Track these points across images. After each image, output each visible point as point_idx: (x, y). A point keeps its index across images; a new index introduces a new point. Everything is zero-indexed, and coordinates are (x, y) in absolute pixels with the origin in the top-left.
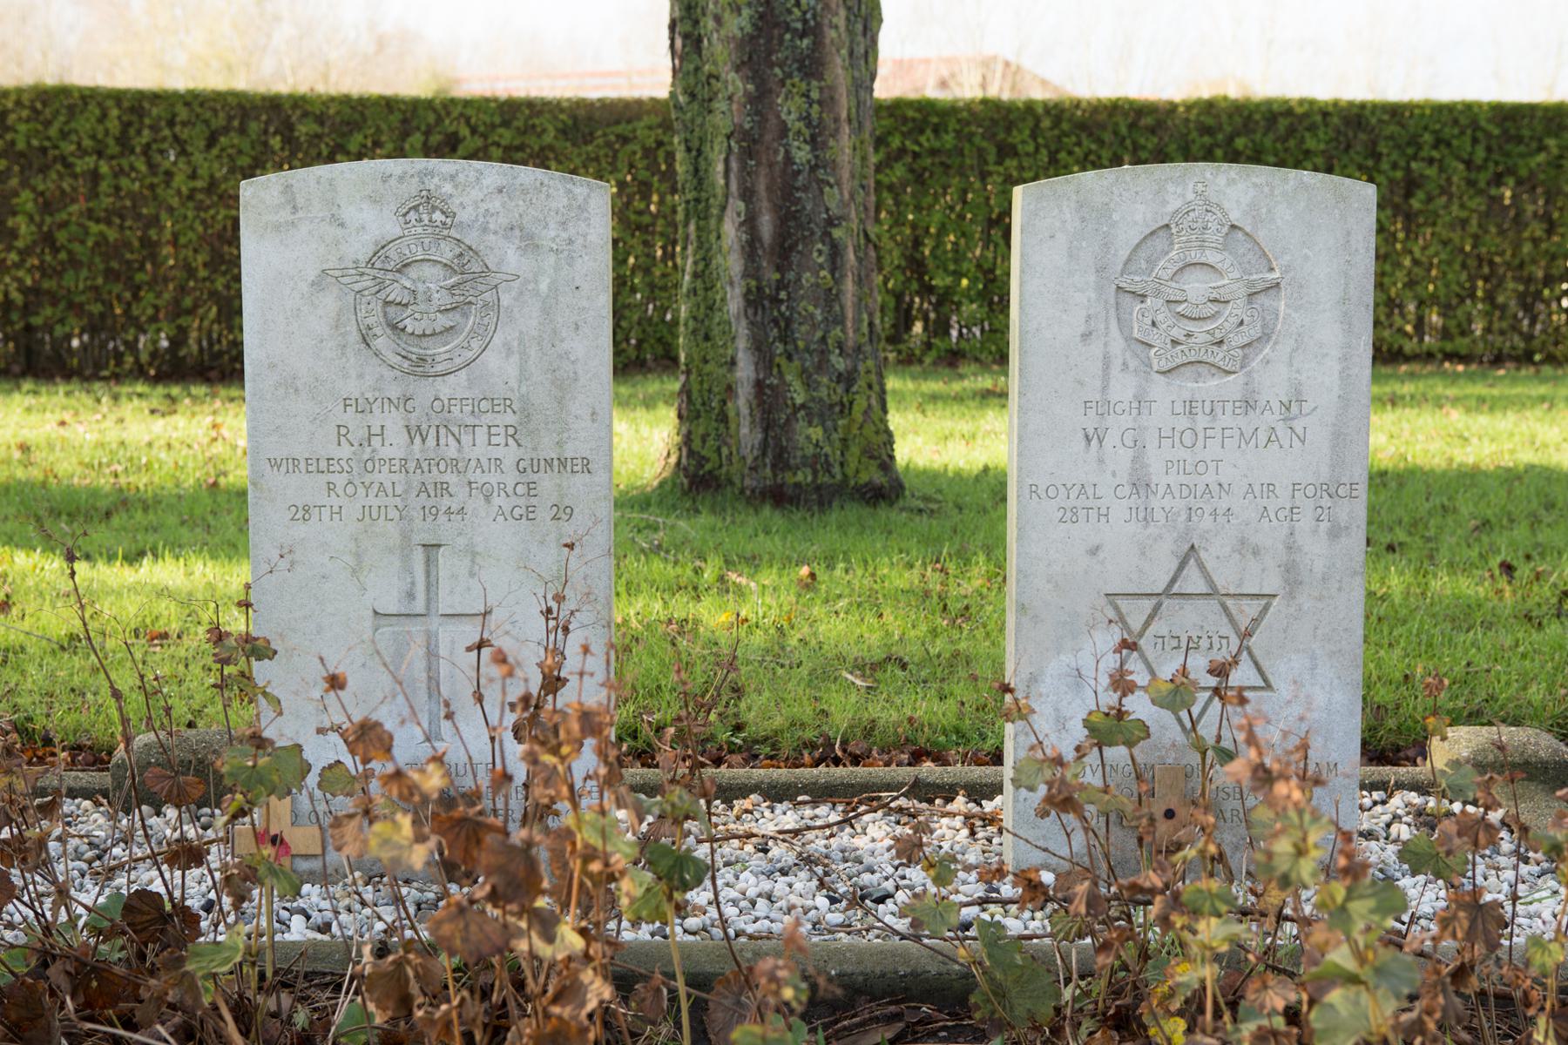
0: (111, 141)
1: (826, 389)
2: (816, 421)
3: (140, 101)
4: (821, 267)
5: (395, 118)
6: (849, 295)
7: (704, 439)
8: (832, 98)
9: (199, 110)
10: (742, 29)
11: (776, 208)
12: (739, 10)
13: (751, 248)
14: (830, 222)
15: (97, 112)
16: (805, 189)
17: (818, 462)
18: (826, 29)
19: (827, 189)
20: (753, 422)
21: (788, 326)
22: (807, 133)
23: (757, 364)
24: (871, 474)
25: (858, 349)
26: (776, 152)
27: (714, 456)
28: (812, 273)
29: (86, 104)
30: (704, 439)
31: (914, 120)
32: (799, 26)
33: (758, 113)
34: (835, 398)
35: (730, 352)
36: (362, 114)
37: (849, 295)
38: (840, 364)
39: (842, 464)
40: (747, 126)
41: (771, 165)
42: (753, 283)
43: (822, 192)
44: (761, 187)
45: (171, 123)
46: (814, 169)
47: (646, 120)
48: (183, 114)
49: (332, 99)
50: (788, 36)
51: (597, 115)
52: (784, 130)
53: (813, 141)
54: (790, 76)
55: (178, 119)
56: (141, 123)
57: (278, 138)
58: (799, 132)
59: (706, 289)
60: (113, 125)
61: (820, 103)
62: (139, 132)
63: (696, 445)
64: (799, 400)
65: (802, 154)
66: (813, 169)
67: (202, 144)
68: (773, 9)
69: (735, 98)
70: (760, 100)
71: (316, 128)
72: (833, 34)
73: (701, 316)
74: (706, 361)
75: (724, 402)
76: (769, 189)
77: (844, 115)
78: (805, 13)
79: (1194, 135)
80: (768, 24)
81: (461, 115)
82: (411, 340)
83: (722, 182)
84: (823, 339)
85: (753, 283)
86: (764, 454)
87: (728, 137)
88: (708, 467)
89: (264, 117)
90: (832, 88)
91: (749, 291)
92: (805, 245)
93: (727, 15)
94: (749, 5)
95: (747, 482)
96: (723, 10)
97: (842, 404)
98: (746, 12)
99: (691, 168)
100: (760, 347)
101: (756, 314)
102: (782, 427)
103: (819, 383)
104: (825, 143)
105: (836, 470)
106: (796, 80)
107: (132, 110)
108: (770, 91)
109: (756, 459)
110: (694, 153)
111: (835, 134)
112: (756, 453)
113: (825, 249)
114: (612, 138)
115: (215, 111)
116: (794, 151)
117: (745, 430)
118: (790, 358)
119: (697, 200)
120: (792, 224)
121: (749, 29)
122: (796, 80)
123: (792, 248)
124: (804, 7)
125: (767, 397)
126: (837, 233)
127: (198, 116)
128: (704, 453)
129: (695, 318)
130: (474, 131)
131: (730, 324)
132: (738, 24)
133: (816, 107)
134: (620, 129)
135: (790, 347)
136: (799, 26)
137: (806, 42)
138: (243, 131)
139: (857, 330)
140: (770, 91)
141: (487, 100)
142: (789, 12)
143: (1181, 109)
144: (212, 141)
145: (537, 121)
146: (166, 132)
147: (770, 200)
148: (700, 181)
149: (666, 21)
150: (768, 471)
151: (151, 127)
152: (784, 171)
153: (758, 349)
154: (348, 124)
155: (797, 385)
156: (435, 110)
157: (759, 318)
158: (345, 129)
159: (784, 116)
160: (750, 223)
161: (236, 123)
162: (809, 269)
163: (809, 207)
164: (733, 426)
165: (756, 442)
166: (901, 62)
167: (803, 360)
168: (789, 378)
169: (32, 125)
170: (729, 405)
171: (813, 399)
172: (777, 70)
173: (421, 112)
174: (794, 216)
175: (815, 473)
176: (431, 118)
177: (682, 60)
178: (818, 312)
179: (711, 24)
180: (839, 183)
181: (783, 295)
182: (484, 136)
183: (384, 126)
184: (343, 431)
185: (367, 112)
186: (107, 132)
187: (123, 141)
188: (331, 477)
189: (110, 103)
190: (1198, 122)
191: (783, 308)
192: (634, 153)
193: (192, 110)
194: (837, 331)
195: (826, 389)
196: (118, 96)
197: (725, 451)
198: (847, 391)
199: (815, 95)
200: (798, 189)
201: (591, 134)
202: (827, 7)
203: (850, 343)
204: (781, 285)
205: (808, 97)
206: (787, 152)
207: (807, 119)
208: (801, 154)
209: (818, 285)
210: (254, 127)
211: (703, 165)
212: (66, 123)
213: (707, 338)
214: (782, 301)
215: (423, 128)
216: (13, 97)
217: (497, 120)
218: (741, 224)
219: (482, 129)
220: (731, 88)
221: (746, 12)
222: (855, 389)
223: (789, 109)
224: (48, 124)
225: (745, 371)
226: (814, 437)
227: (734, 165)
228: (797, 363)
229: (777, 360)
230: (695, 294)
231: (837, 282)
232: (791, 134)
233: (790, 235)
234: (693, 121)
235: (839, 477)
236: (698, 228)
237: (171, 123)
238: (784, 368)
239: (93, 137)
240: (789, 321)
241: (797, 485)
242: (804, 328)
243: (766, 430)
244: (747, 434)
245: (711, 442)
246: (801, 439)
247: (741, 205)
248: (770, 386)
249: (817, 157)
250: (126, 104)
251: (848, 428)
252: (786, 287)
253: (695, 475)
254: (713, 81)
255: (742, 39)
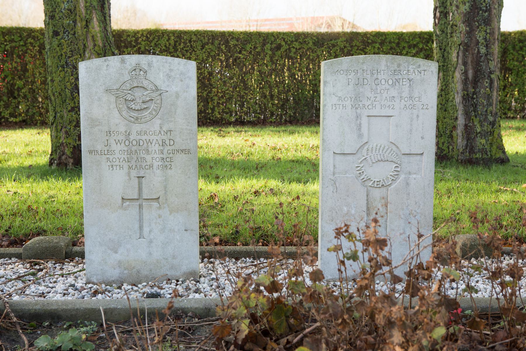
0: (171, 47)
1: (487, 127)
2: (483, 137)
3: (180, 34)
4: (487, 87)
5: (261, 39)
6: (495, 96)
7: (443, 143)
8: (493, 32)
9: (199, 37)
10: (466, 10)
11: (474, 68)
12: (465, 4)
13: (465, 81)
14: (491, 73)
15: (167, 38)
16: (483, 62)
17: (483, 151)
18: (492, 9)
19: (490, 62)
20: (463, 138)
21: (476, 106)
22: (485, 43)
23: (465, 119)
24: (500, 155)
25: (496, 114)
26: (475, 50)
27: (447, 149)
28: (484, 89)
29: (164, 35)
30: (443, 143)
31: (426, 38)
32: (485, 8)
33: (470, 37)
34: (489, 130)
35: (456, 115)
36: (251, 38)
37: (495, 96)
38: (491, 119)
39: (490, 152)
40: (466, 41)
41: (473, 54)
42: (466, 93)
43: (488, 62)
44: (469, 62)
45: (190, 41)
46: (486, 55)
47: (341, 39)
48: (194, 38)
49: (241, 33)
50: (481, 12)
51: (325, 37)
52: (478, 42)
53: (487, 46)
54: (481, 25)
55: (192, 40)
56: (181, 41)
57: (224, 46)
58: (483, 43)
59: (446, 95)
60: (172, 42)
61: (490, 34)
62: (180, 44)
63: (441, 145)
64: (478, 131)
65: (483, 50)
66: (486, 55)
67: (199, 48)
68: (476, 3)
69: (462, 32)
70: (470, 33)
71: (236, 42)
72: (495, 11)
73: (443, 103)
74: (445, 118)
75: (452, 132)
76: (472, 62)
77: (496, 38)
78: (487, 4)
79: (517, 43)
80: (475, 8)
81: (282, 38)
82: (134, 111)
83: (456, 60)
84: (486, 111)
85: (466, 93)
86: (466, 148)
87: (459, 45)
88: (445, 152)
89: (220, 39)
90: (493, 29)
91: (464, 95)
92: (482, 80)
93: (461, 5)
94: (468, 2)
95: (460, 157)
96: (460, 3)
97: (491, 132)
98: (467, 4)
99: (442, 55)
100: (467, 114)
101: (466, 103)
102: (473, 140)
103: (484, 125)
104: (490, 47)
105: (489, 153)
106: (483, 26)
107: (178, 37)
108: (474, 30)
109: (464, 150)
110: (443, 50)
111: (494, 44)
112: (464, 148)
113: (488, 81)
114: (330, 45)
115: (204, 37)
116: (480, 49)
117: (460, 140)
118: (476, 117)
119: (443, 66)
120: (479, 73)
121: (468, 10)
122: (483, 26)
123: (478, 81)
124: (486, 2)
125: (468, 129)
126: (493, 76)
127: (199, 38)
128: (443, 148)
129: (441, 104)
130: (286, 43)
131: (456, 106)
132: (465, 8)
133: (488, 35)
134: (332, 42)
135: (476, 113)
136: (485, 8)
137: (486, 14)
138: (212, 44)
139: (496, 108)
140: (474, 30)
141: (291, 33)
142: (482, 4)
143: (513, 34)
144: (203, 47)
145: (306, 40)
146: (188, 44)
147: (472, 66)
148: (445, 60)
149: (433, 7)
150: (468, 153)
151: (184, 43)
152: (477, 56)
153: (466, 114)
154: (246, 41)
155: (478, 126)
156: (274, 36)
157: (467, 104)
158: (245, 43)
159: (478, 38)
160: (465, 73)
161: (211, 41)
162: (483, 88)
163: (484, 68)
164: (455, 140)
165: (464, 145)
166: (314, 17)
167: (480, 118)
168: (475, 123)
169: (146, 42)
170: (454, 132)
171: (482, 130)
172: (476, 23)
173: (270, 37)
174: (479, 71)
175: (482, 154)
176: (273, 39)
177: (439, 20)
178: (485, 102)
179: (454, 8)
180: (494, 60)
181: (475, 96)
182: (289, 45)
183: (258, 42)
184: (164, 141)
185: (252, 37)
186: (170, 44)
187: (175, 47)
188: (108, 156)
189: (171, 35)
190: (518, 38)
191: (475, 101)
192: (337, 50)
193: (197, 37)
194: (491, 108)
195: (487, 127)
196: (174, 32)
197: (451, 147)
198: (492, 128)
199: (488, 31)
200: (481, 62)
201: (323, 44)
202: (493, 2)
203: (494, 112)
204: (474, 93)
205: (486, 32)
206: (478, 50)
207: (485, 39)
208: (483, 50)
209: (485, 93)
210: (217, 42)
211: (446, 54)
212: (157, 41)
213: (445, 110)
214: (474, 98)
215: (270, 42)
216: (141, 33)
217: (294, 39)
218: (462, 73)
219: (289, 42)
220: (461, 29)
221: (467, 4)
222: (495, 127)
223: (480, 36)
224: (151, 42)
225: (461, 121)
226: (482, 143)
227: (461, 54)
228: (478, 118)
229: (472, 117)
230: (442, 96)
231: (491, 92)
232: (480, 44)
233: (478, 77)
234: (442, 40)
235: (489, 156)
236: (444, 75)
237: (190, 41)
238: (474, 120)
239: (165, 46)
240: (476, 105)
241: (477, 158)
242: (481, 107)
243: (467, 141)
244: (460, 141)
245: (446, 144)
246: (478, 143)
247: (463, 67)
248: (470, 126)
249: (487, 51)
250: (176, 35)
251: (492, 140)
252: (476, 94)
253: (440, 155)
254: (454, 27)
255: (466, 13)
